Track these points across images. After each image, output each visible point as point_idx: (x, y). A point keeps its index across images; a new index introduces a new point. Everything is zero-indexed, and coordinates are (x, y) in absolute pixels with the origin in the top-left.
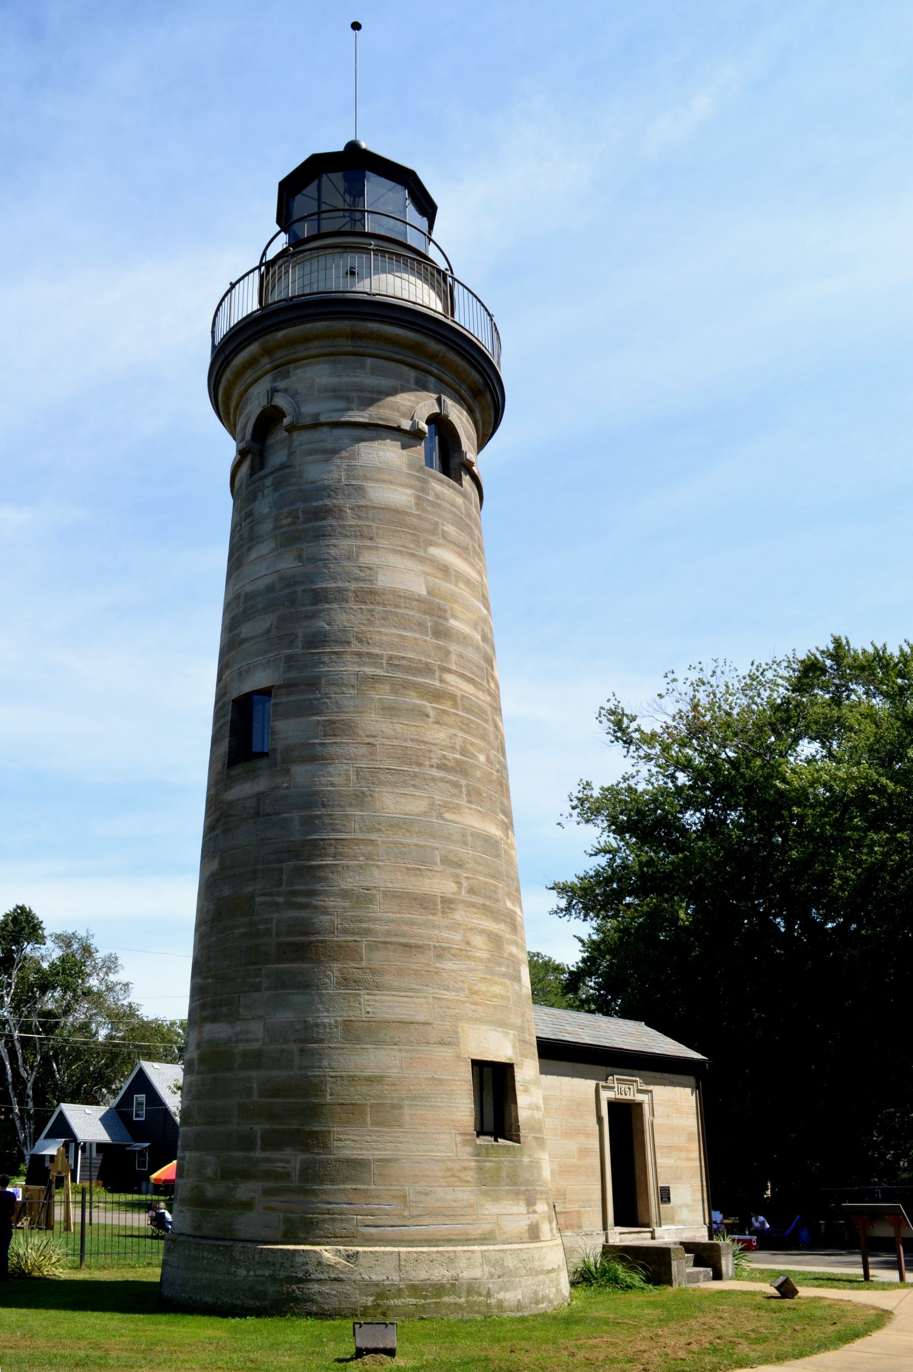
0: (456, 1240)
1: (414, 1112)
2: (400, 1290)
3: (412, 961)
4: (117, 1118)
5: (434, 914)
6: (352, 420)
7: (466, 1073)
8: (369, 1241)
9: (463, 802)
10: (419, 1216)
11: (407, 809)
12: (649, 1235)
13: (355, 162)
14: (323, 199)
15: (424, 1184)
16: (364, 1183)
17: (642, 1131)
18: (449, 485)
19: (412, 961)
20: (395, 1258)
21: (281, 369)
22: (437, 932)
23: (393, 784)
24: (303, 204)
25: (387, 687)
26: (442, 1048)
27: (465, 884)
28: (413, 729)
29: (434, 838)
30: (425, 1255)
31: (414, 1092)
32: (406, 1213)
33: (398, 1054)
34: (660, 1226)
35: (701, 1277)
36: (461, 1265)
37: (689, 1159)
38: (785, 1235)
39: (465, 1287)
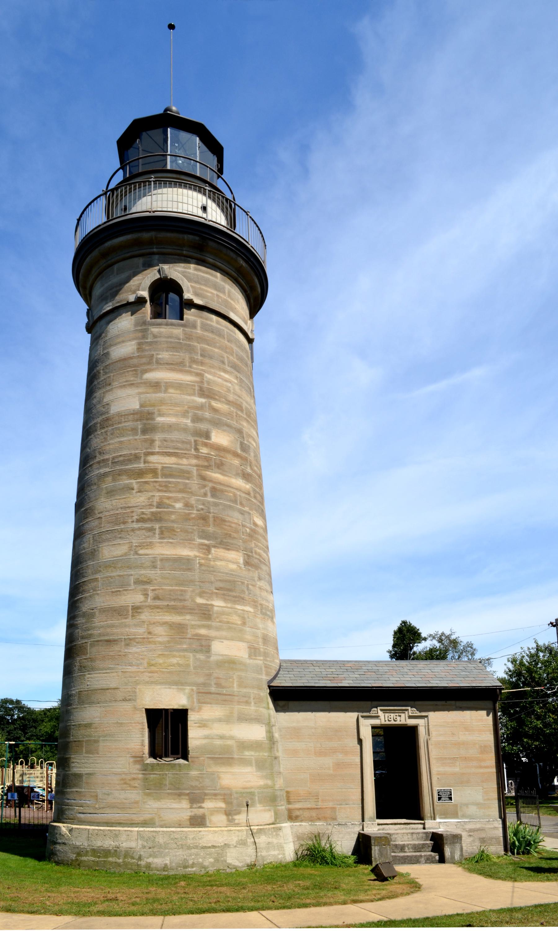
0: (124, 824)
1: (105, 744)
2: (87, 852)
3: (111, 650)
5: (126, 618)
6: (105, 311)
8: (81, 822)
9: (156, 539)
10: (103, 808)
11: (115, 554)
12: (422, 826)
15: (108, 788)
16: (80, 788)
18: (167, 325)
19: (111, 650)
20: (87, 832)
22: (127, 630)
23: (108, 540)
25: (110, 479)
26: (124, 703)
27: (151, 594)
28: (122, 501)
29: (131, 568)
30: (102, 832)
31: (106, 732)
32: (97, 806)
33: (98, 709)
34: (435, 819)
35: (423, 860)
36: (122, 839)
39: (123, 853)
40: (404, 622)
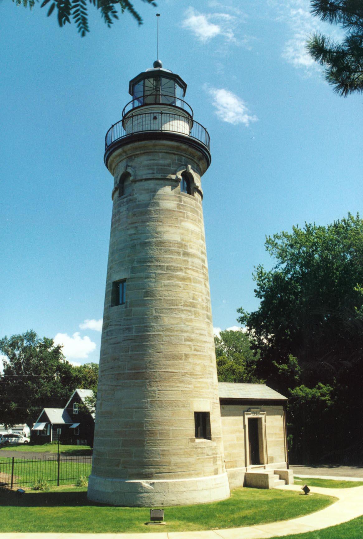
7: (193, 417)
9: (193, 317)
13: (157, 75)
17: (262, 429)
21: (130, 158)
24: (139, 87)
37: (280, 438)
38: (314, 461)
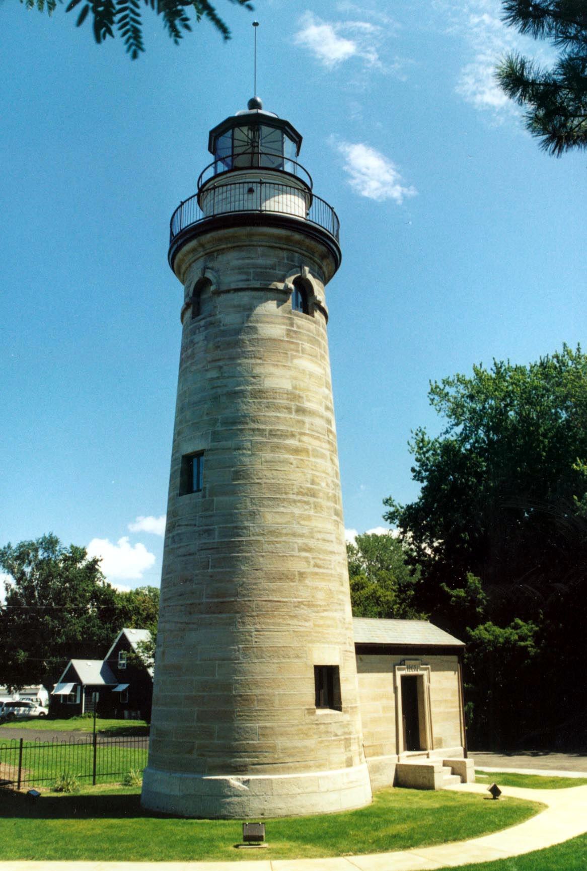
4: (110, 670)
7: (311, 674)
9: (312, 512)
13: (254, 121)
14: (235, 137)
17: (423, 692)
21: (210, 255)
24: (225, 141)
37: (452, 707)
40: (356, 644)
